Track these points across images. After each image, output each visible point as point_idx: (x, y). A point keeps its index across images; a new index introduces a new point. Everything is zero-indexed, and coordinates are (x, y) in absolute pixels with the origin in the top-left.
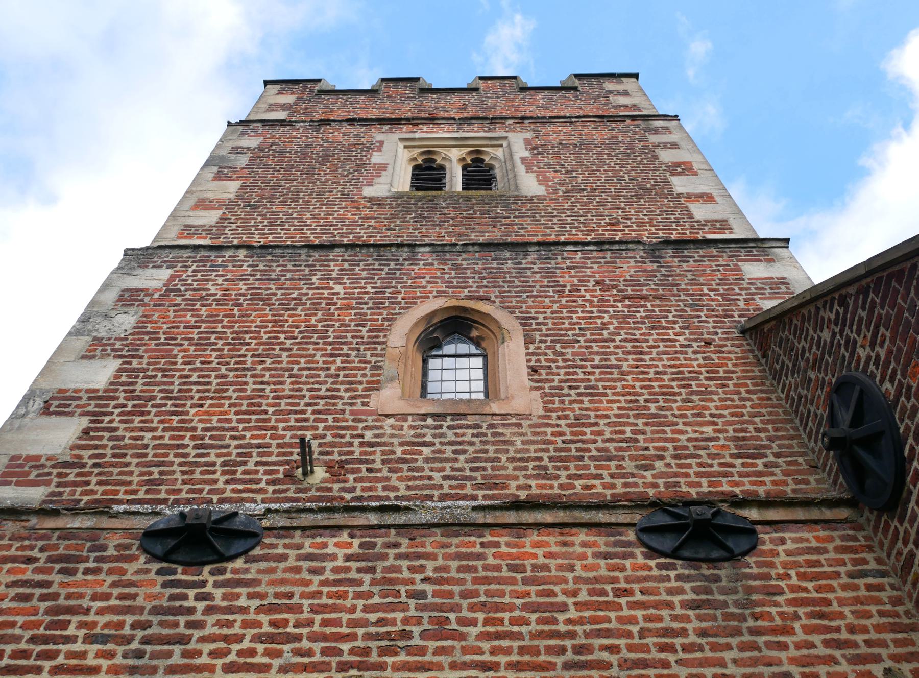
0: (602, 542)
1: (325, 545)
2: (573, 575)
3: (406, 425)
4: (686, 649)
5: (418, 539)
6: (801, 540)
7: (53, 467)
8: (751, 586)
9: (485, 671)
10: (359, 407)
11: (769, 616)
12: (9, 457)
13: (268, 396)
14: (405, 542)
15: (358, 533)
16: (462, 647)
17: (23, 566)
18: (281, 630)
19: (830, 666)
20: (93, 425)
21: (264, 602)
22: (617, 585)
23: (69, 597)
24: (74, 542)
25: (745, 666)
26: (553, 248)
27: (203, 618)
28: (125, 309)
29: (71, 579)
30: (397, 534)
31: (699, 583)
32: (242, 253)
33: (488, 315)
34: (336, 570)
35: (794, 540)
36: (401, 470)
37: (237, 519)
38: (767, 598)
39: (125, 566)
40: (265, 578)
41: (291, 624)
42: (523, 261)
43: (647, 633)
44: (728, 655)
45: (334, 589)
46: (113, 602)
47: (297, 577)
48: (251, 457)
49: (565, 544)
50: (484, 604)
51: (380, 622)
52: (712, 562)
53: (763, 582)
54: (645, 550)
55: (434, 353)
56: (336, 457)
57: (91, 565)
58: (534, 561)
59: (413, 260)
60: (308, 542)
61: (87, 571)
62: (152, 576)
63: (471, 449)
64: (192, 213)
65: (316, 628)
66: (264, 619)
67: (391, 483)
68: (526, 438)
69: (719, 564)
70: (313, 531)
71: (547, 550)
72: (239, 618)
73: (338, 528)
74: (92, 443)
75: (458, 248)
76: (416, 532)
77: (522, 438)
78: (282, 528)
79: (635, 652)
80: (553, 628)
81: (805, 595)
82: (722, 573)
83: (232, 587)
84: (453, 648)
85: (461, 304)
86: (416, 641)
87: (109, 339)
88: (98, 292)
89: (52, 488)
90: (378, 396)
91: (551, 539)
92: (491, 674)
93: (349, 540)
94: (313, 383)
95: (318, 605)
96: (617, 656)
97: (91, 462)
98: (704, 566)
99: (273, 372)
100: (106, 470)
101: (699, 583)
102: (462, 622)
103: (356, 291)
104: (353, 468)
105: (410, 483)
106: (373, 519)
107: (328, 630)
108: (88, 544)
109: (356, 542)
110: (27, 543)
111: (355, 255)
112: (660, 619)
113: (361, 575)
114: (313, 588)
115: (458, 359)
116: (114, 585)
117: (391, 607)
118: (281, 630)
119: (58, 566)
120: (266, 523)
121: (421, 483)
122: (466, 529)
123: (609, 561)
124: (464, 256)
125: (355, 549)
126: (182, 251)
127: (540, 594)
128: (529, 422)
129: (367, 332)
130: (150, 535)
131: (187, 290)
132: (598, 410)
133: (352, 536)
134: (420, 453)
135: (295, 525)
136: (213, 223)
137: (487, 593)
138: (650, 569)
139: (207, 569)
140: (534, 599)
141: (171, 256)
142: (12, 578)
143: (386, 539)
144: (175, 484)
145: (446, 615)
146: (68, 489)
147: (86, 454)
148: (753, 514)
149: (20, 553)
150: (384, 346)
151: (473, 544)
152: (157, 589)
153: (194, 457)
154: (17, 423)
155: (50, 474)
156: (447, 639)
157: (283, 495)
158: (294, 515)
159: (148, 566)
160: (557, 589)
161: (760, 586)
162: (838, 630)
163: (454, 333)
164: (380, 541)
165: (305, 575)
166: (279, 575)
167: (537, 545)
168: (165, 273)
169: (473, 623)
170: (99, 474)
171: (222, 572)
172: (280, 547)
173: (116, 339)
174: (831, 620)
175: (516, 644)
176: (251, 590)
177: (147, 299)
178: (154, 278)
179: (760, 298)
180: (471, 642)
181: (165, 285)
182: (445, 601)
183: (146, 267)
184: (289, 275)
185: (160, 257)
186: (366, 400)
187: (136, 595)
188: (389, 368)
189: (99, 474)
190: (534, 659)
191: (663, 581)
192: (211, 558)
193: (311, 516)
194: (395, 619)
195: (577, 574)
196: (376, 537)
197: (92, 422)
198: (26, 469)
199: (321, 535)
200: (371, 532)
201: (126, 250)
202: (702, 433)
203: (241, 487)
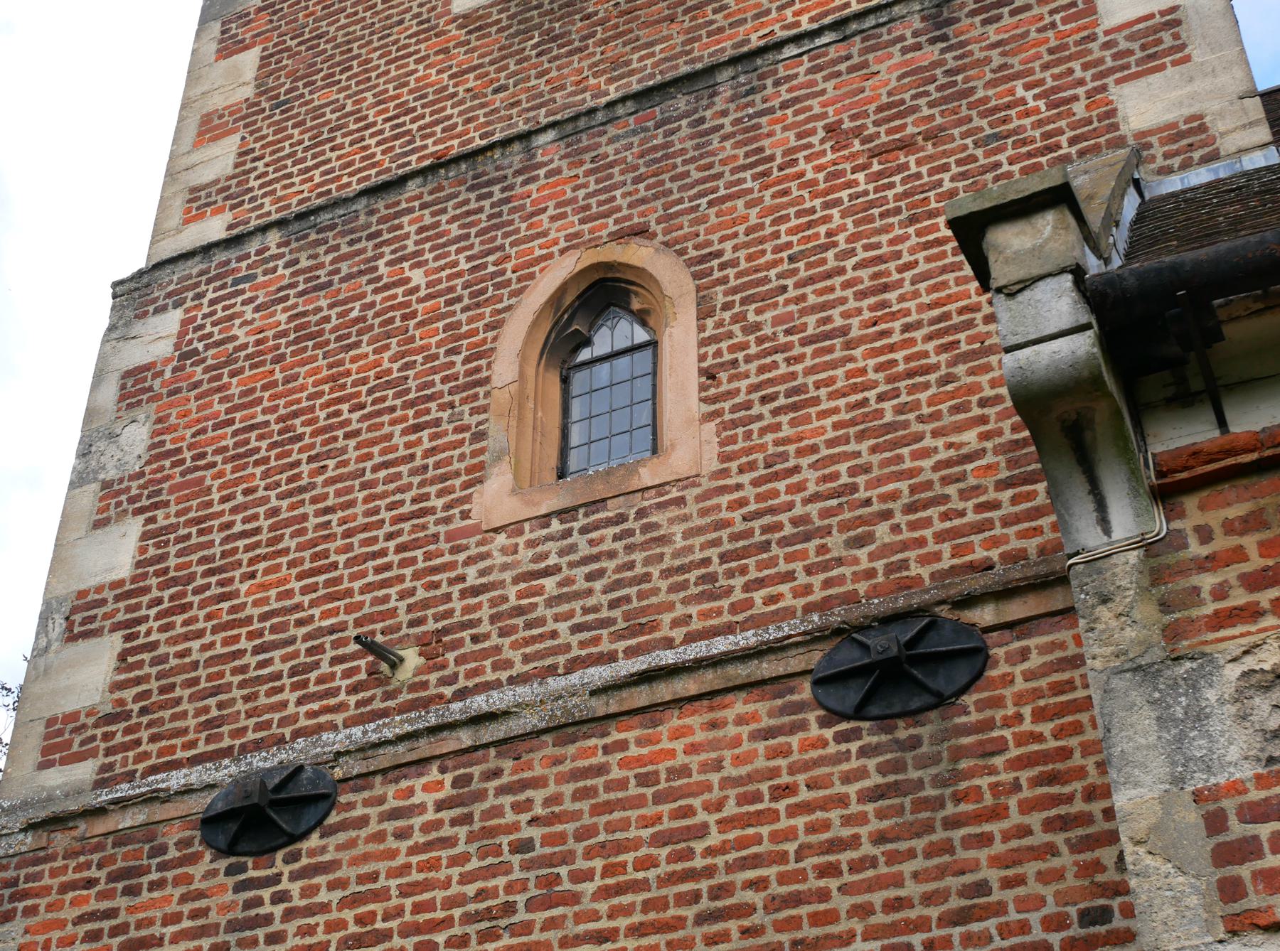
0: (762, 709)
1: (410, 792)
2: (719, 775)
3: (521, 541)
4: (855, 867)
5: (525, 758)
6: (1054, 646)
7: (96, 726)
8: (960, 747)
9: (601, 943)
10: (458, 524)
11: (977, 793)
12: (44, 722)
13: (335, 535)
14: (508, 764)
15: (450, 763)
16: (576, 914)
17: (85, 892)
18: (369, 928)
19: (1044, 860)
20: (128, 645)
21: (347, 893)
22: (775, 782)
23: (139, 925)
24: (130, 847)
25: (927, 881)
26: (759, 62)
27: (282, 927)
28: (132, 414)
29: (138, 900)
30: (499, 755)
31: (889, 756)
32: (273, 237)
33: (643, 270)
34: (426, 828)
35: (1043, 650)
36: (514, 629)
37: (304, 776)
38: (981, 762)
39: (190, 870)
40: (345, 856)
41: (379, 918)
42: (708, 113)
43: (806, 851)
44: (908, 868)
45: (424, 857)
46: (187, 924)
47: (382, 847)
48: (324, 652)
49: (713, 725)
50: (603, 845)
51: (481, 895)
52: (912, 715)
53: (980, 737)
54: (821, 712)
55: (585, 355)
56: (431, 626)
57: (154, 876)
58: (669, 764)
59: (527, 170)
60: (391, 790)
61: (153, 886)
62: (221, 878)
63: (610, 565)
64: (196, 157)
65: (408, 917)
66: (348, 915)
67: (503, 656)
68: (691, 524)
69: (921, 717)
70: (397, 772)
71: (689, 740)
72: (320, 919)
73: (424, 762)
74: (132, 675)
75: (600, 116)
76: (522, 746)
77: (685, 526)
78: (358, 776)
79: (787, 884)
80: (688, 865)
81: (1035, 747)
82: (924, 731)
83: (310, 877)
84: (564, 917)
85: (601, 259)
86: (521, 916)
87: (121, 480)
88: (152, 243)
89: (101, 760)
90: (482, 494)
91: (695, 721)
92: (609, 946)
93: (440, 777)
94: (394, 493)
95: (408, 884)
96: (763, 894)
97: (136, 707)
98: (901, 723)
99: (339, 485)
100: (156, 716)
101: (889, 756)
102: (577, 877)
103: (444, 274)
104: (453, 641)
105: (528, 650)
106: (465, 738)
107: (421, 918)
108: (147, 847)
109: (448, 778)
110: (82, 859)
111: (440, 188)
112: (826, 825)
113: (456, 829)
114: (401, 860)
115: (628, 344)
116: (184, 899)
117: (491, 872)
118: (369, 928)
119: (120, 886)
120: (338, 773)
121: (542, 646)
122: (585, 728)
123: (771, 742)
124: (612, 131)
125: (447, 791)
126: (190, 263)
127: (676, 815)
128: (697, 491)
129: (465, 362)
130: (210, 822)
131: (207, 347)
132: (801, 439)
133: (443, 770)
134: (539, 591)
135: (372, 768)
136: (230, 171)
137: (610, 828)
138: (825, 744)
139: (280, 855)
140: (667, 824)
141: (175, 278)
142: (77, 912)
143: (483, 767)
144: (237, 721)
145: (555, 870)
146: (119, 757)
147: (128, 694)
148: (985, 615)
149: (78, 876)
150: (487, 388)
151: (592, 751)
152: (229, 896)
153: (256, 668)
154: (41, 662)
155: (93, 738)
156: (557, 905)
157: (369, 708)
158: (370, 753)
159: (214, 866)
160: (697, 802)
161: (972, 745)
162: (1069, 799)
163: (608, 307)
164: (476, 771)
165: (391, 843)
166: (362, 849)
167: (676, 735)
168: (171, 320)
169: (588, 876)
170: (149, 725)
171: (295, 857)
172: (359, 805)
173: (132, 478)
174: (1064, 783)
175: (639, 898)
176: (331, 877)
177: (157, 384)
178: (159, 336)
179: (1118, 82)
180: (586, 904)
181: (177, 346)
182: (557, 849)
183: (146, 314)
184: (345, 268)
185: (161, 287)
186: (466, 507)
187: (208, 909)
188: (498, 433)
189: (149, 725)
190: (661, 915)
191: (839, 762)
192: (281, 841)
193: (390, 750)
194: (496, 887)
195: (724, 773)
196: (471, 765)
197: (128, 638)
198: (67, 736)
199: (405, 777)
200: (465, 758)
201: (115, 285)
202: (959, 446)
203: (315, 706)
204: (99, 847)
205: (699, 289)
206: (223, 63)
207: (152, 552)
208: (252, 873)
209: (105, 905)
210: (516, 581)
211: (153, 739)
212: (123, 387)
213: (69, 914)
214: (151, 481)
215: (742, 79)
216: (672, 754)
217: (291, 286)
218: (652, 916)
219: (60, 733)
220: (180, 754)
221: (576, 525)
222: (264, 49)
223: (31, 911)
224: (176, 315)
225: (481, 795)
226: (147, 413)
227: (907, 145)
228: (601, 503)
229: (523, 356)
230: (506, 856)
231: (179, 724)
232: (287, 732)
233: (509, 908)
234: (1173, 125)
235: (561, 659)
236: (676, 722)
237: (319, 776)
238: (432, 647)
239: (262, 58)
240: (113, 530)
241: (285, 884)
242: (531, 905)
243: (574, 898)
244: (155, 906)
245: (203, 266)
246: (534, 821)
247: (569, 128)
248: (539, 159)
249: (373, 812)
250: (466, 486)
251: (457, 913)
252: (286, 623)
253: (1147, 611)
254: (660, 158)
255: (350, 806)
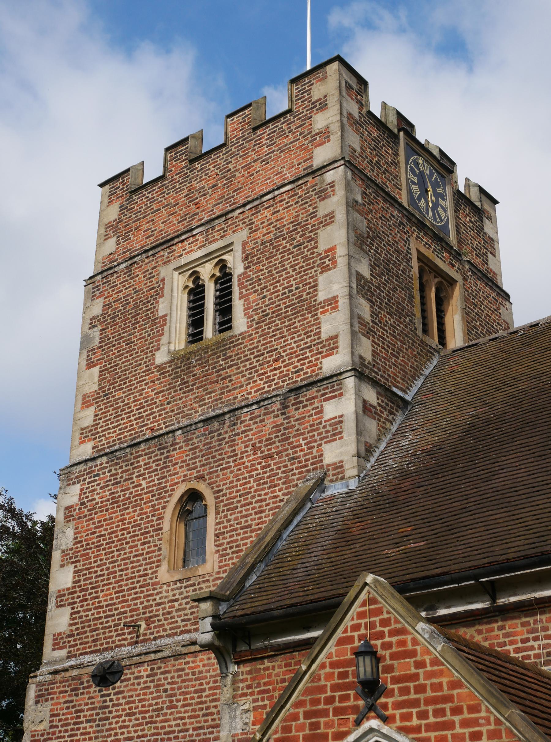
3: (170, 588)
7: (66, 638)
14: (163, 665)
15: (149, 663)
26: (237, 412)
30: (161, 662)
50: (183, 692)
57: (81, 691)
60: (136, 670)
64: (81, 415)
66: (127, 707)
86: (165, 711)
106: (152, 656)
109: (149, 668)
120: (123, 664)
124: (197, 433)
125: (149, 672)
130: (94, 676)
133: (148, 666)
134: (173, 607)
136: (92, 423)
139: (111, 687)
147: (74, 628)
152: (99, 699)
164: (155, 666)
171: (114, 689)
175: (190, 708)
179: (326, 443)
180: (179, 709)
181: (79, 499)
193: (135, 658)
197: (73, 608)
204: (67, 681)
205: (216, 503)
206: (88, 371)
207: (77, 578)
208: (104, 692)
209: (70, 699)
210: (169, 602)
211: (81, 644)
212: (65, 514)
213: (62, 700)
214: (75, 552)
215: (232, 419)
216: (199, 666)
217: (110, 481)
218: (193, 713)
219: (57, 639)
220: (88, 650)
221: (183, 585)
222: (100, 368)
223: (52, 699)
224: (78, 487)
225: (156, 674)
226: (72, 524)
227: (271, 456)
228: (188, 579)
229: (171, 521)
230: (162, 693)
231: (87, 640)
232: (113, 645)
233: (162, 708)
234: (335, 464)
235: (178, 630)
236: (201, 657)
237: (119, 664)
238: (148, 620)
239: (100, 372)
240: (65, 568)
241: (112, 697)
242: (167, 708)
243: (176, 707)
244: (82, 700)
245: (85, 467)
246: (168, 683)
247: (185, 429)
248: (177, 441)
249: (132, 676)
250: (157, 567)
251: (151, 708)
252: (112, 609)
253: (231, 690)
254: (209, 446)
255: (127, 674)
